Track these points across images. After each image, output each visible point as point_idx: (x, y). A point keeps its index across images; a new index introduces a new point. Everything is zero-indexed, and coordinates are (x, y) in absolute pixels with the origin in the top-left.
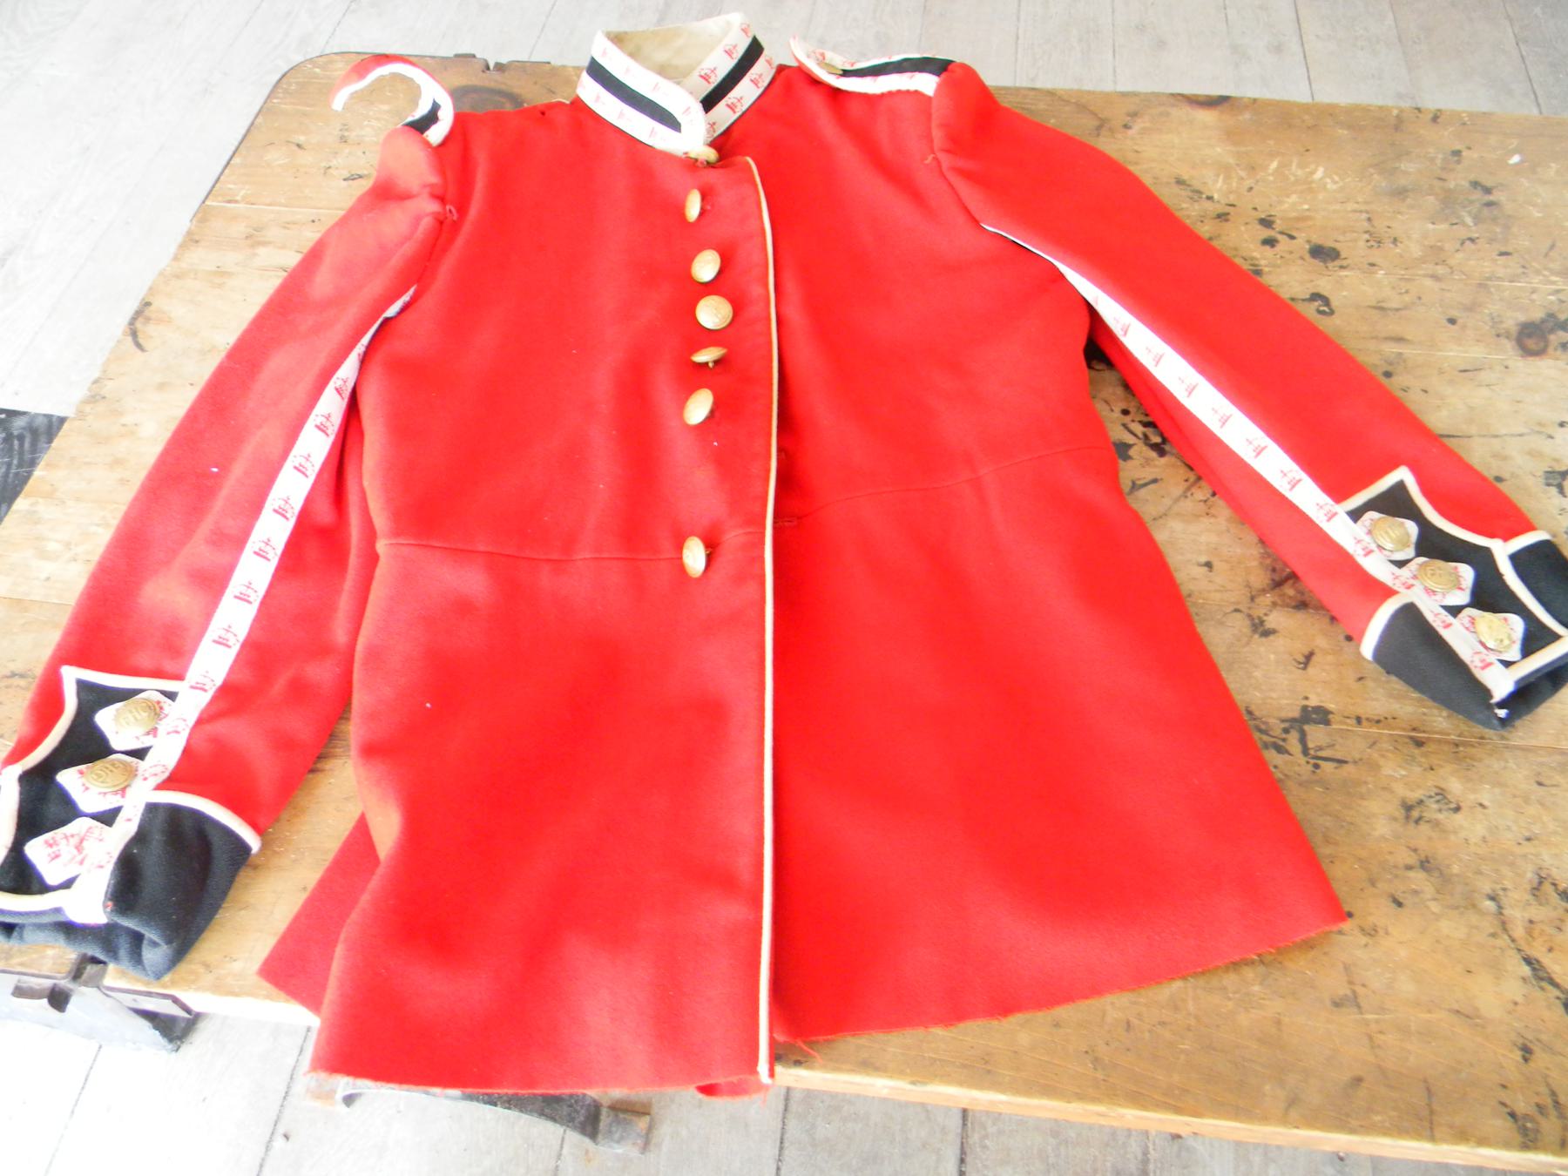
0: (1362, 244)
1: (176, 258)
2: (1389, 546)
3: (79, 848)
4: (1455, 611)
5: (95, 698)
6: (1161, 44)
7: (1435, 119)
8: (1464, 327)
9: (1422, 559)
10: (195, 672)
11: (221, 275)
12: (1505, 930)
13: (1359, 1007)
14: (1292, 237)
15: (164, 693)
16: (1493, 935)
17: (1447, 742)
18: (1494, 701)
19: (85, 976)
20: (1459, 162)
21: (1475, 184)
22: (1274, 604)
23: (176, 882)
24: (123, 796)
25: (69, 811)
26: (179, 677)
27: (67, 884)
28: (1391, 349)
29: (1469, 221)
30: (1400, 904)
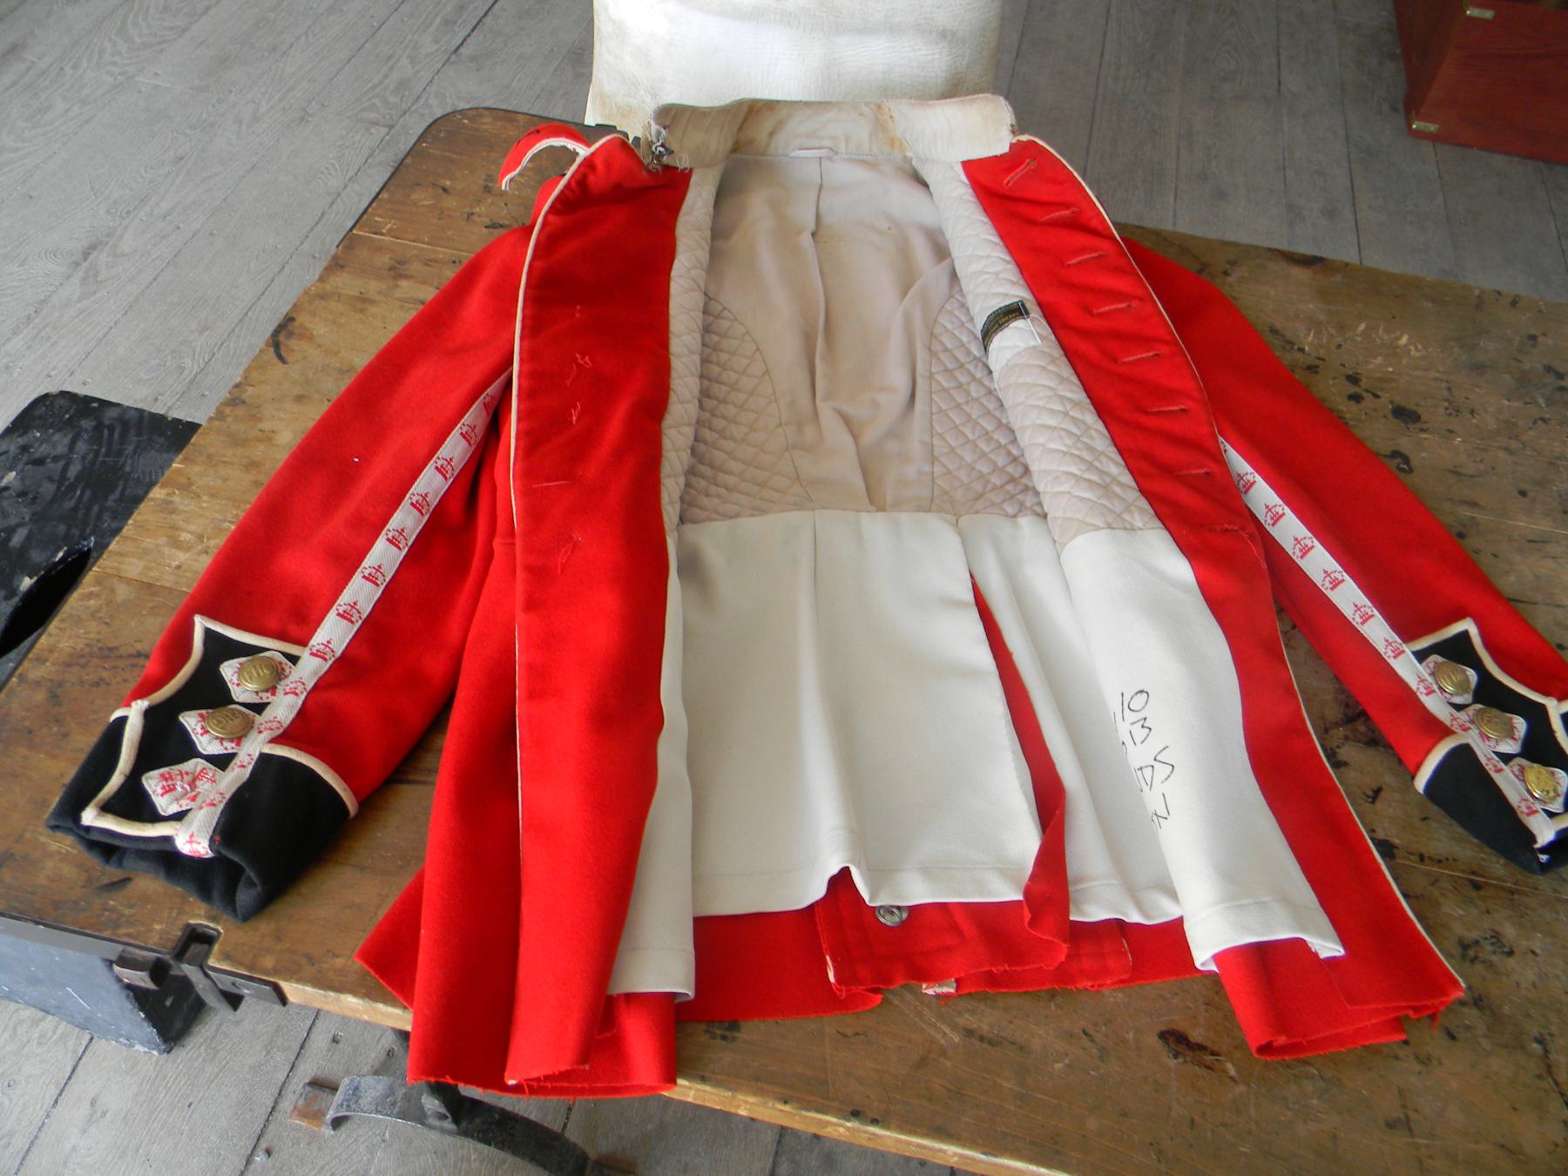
0: (1441, 411)
1: (321, 280)
2: (1450, 689)
3: (192, 784)
4: (1506, 758)
5: (220, 649)
6: (1220, 195)
7: (1514, 303)
8: (1533, 500)
9: (1479, 706)
11: (363, 301)
12: (1550, 1073)
13: (1410, 1129)
14: (1377, 396)
15: (286, 655)
16: (1539, 1077)
17: (1503, 889)
18: (1538, 846)
19: (187, 955)
20: (1534, 346)
21: (1549, 369)
22: (1347, 738)
23: (281, 837)
24: (238, 744)
25: (187, 750)
27: (179, 817)
28: (1466, 512)
29: (1541, 401)
30: (1453, 1037)
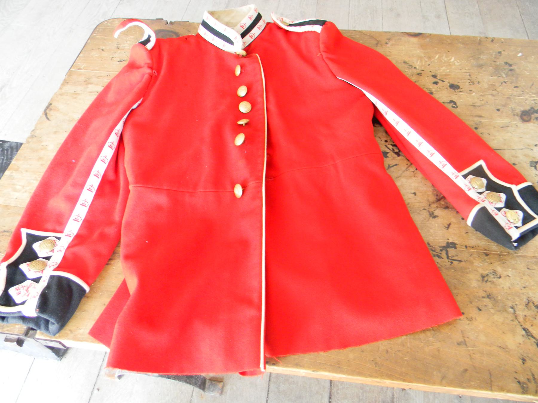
0: (467, 83)
1: (60, 89)
2: (476, 187)
3: (27, 291)
4: (499, 209)
5: (33, 239)
6: (398, 15)
7: (492, 41)
8: (502, 112)
9: (488, 192)
10: (67, 230)
11: (76, 94)
12: (516, 319)
13: (466, 345)
14: (443, 81)
15: (56, 238)
16: (512, 320)
17: (497, 254)
18: (513, 240)
19: (29, 335)
20: (500, 56)
21: (506, 63)
22: (437, 207)
23: (60, 302)
24: (42, 273)
25: (24, 278)
26: (62, 232)
27: (23, 303)
28: (477, 120)
29: (504, 76)
30: (480, 310)
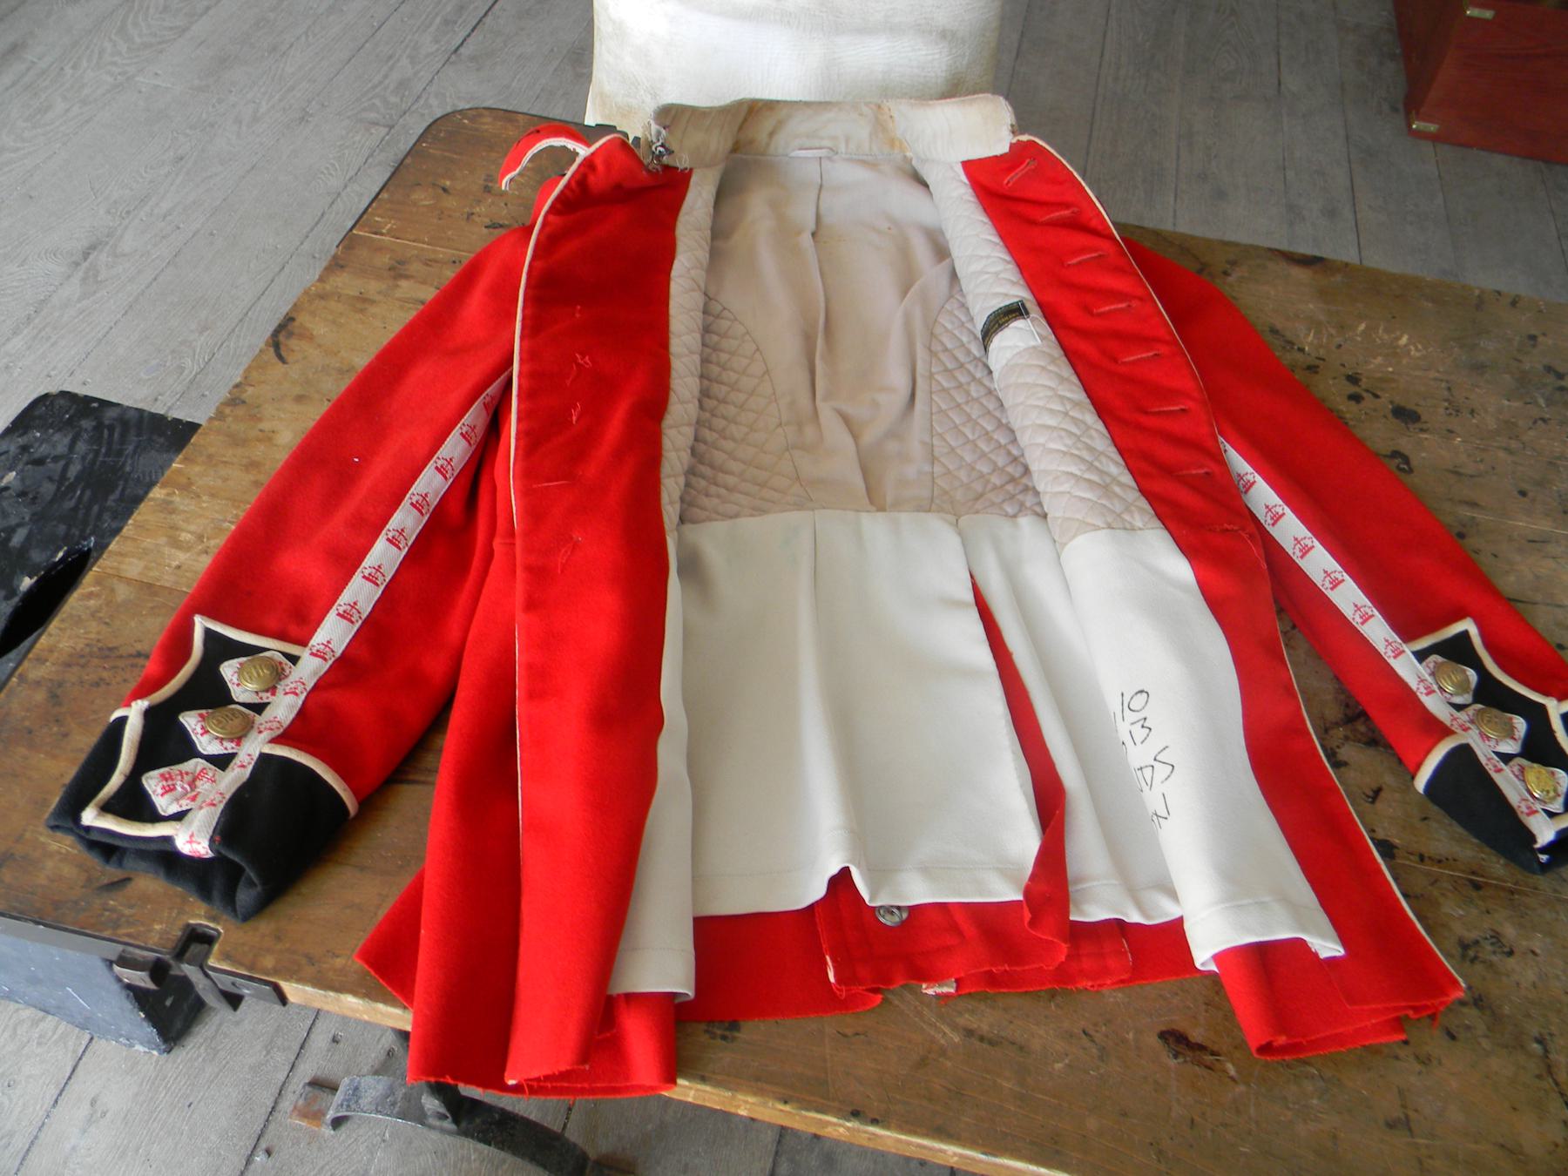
0: (1441, 411)
1: (321, 280)
2: (1450, 689)
3: (192, 784)
4: (1506, 758)
5: (220, 649)
7: (1514, 303)
8: (1533, 500)
9: (1479, 706)
10: (318, 639)
11: (363, 301)
12: (1550, 1073)
13: (1410, 1129)
14: (1377, 396)
15: (286, 655)
16: (1539, 1077)
17: (1503, 889)
18: (1538, 846)
19: (187, 955)
20: (1534, 346)
21: (1549, 369)
22: (1347, 738)
23: (281, 837)
24: (238, 744)
25: (187, 750)
26: (303, 643)
27: (179, 817)
28: (1466, 512)
29: (1541, 401)
30: (1453, 1037)
